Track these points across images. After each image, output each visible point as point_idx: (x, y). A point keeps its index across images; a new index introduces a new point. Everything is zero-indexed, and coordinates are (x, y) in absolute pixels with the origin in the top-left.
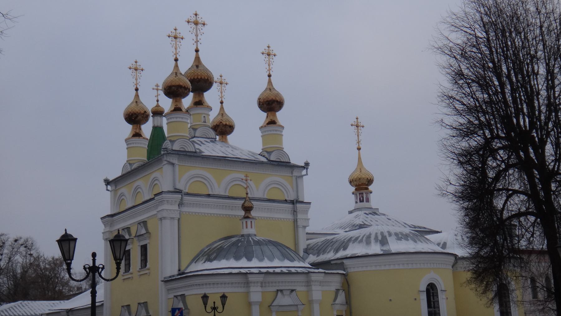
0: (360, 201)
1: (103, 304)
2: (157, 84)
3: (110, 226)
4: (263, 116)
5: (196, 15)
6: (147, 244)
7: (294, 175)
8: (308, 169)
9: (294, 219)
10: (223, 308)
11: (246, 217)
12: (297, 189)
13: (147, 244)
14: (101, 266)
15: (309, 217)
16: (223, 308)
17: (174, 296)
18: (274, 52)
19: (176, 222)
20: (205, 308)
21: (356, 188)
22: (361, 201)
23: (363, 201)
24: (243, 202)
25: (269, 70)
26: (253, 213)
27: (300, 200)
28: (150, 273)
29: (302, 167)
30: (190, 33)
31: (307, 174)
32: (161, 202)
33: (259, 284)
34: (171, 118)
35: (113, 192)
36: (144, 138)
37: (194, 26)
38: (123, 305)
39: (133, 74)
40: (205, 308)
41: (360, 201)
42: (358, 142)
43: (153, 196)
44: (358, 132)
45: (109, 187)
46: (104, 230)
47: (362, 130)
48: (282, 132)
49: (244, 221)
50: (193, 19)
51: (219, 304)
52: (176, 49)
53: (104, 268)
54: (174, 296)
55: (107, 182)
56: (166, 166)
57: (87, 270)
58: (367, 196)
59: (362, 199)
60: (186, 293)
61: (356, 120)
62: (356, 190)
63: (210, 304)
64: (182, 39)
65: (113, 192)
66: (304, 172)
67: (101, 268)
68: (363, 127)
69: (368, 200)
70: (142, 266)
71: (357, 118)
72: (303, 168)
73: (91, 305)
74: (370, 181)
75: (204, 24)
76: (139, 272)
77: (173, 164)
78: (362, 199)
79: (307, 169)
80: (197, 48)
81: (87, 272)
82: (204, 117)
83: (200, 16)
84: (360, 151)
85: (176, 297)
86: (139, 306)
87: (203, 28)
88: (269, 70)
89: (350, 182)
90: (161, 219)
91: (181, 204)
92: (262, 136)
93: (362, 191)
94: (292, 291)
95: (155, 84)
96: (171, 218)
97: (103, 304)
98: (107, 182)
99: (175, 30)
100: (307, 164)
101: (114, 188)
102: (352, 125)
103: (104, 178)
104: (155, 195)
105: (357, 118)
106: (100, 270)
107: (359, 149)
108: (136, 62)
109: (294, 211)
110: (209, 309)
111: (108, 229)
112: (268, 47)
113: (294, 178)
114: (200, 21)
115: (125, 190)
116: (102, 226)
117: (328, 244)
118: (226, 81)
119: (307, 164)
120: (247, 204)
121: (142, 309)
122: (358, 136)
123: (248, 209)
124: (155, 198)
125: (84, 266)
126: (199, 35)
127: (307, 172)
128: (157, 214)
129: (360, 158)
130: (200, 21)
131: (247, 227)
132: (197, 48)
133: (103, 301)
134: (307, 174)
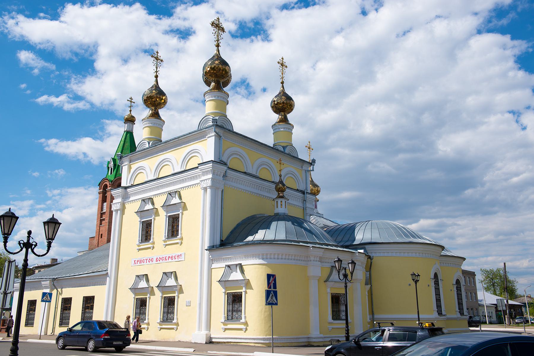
2: (131, 98)
4: (275, 117)
7: (303, 169)
9: (304, 208)
14: (34, 243)
17: (226, 266)
18: (286, 64)
31: (313, 170)
39: (154, 62)
49: (279, 200)
52: (157, 68)
53: (37, 246)
54: (226, 266)
57: (22, 245)
58: (315, 203)
60: (243, 263)
67: (34, 245)
73: (26, 278)
81: (21, 246)
85: (229, 266)
86: (165, 276)
95: (130, 97)
100: (314, 161)
106: (33, 246)
113: (304, 172)
119: (314, 161)
124: (199, 168)
125: (19, 242)
127: (313, 168)
128: (200, 183)
134: (313, 170)
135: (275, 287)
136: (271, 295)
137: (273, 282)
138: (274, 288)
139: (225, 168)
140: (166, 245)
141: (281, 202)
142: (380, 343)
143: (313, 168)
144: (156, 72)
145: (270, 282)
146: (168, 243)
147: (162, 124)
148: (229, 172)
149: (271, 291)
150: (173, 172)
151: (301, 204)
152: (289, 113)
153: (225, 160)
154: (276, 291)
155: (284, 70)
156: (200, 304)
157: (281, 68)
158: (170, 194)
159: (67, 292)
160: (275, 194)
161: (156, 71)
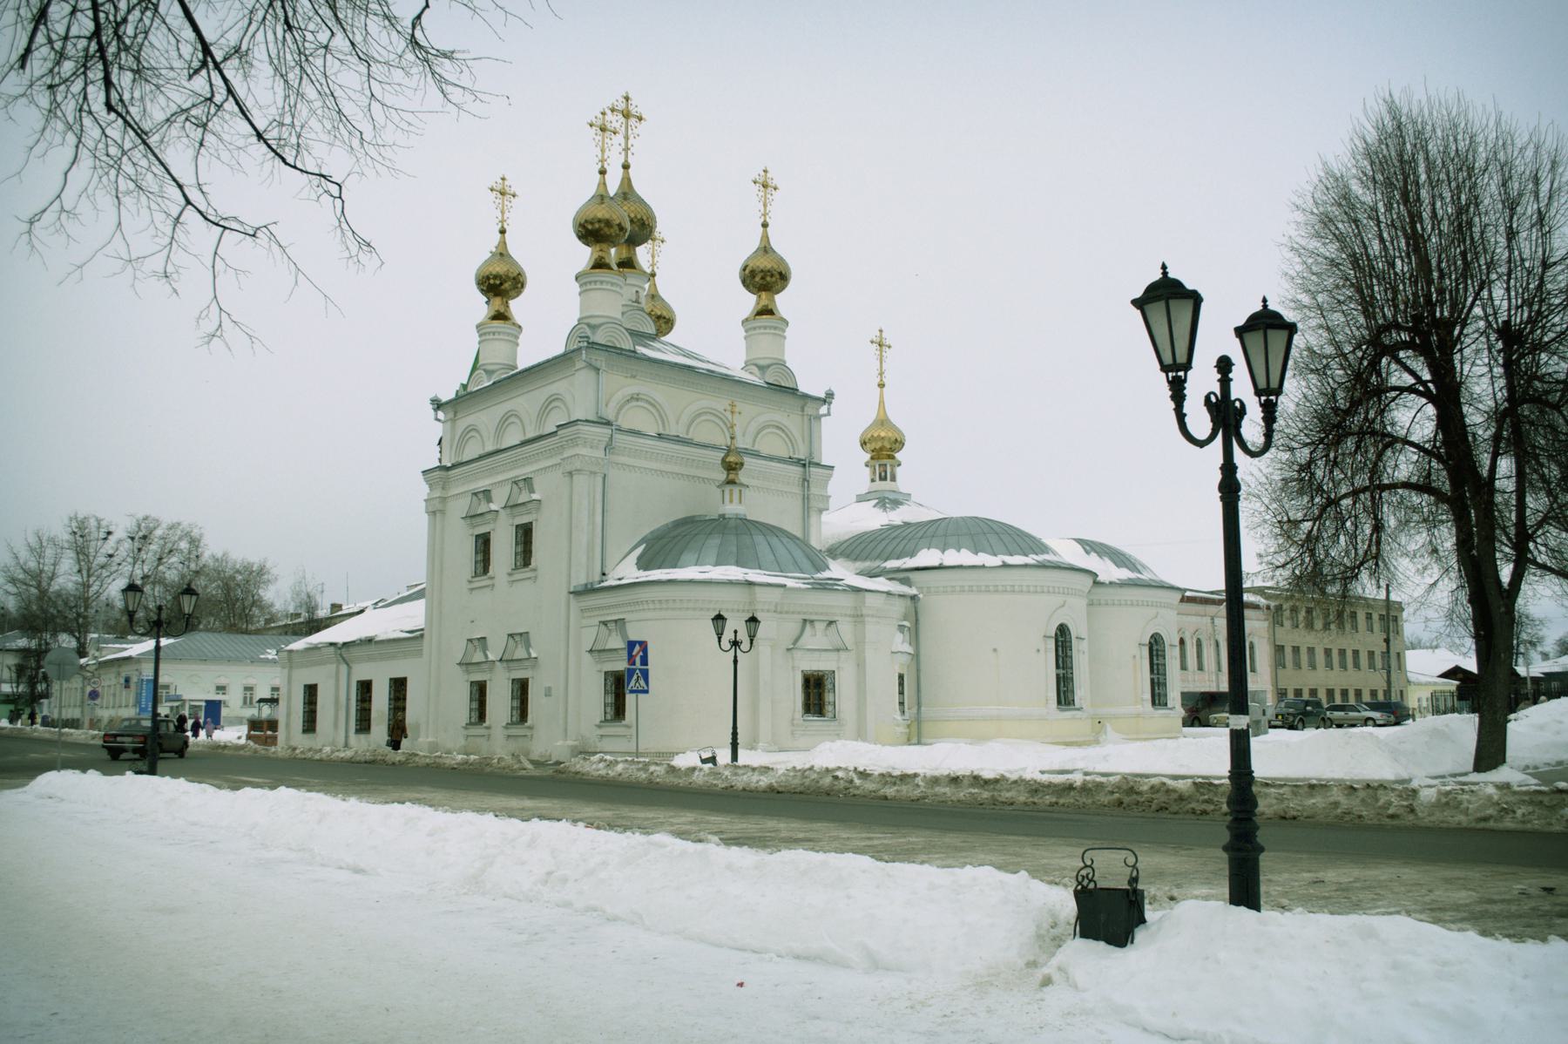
0: (881, 479)
1: (422, 636)
3: (443, 488)
5: (627, 99)
6: (531, 523)
8: (832, 406)
10: (751, 643)
11: (731, 482)
12: (811, 437)
13: (531, 523)
15: (829, 494)
16: (751, 643)
18: (775, 182)
19: (599, 480)
20: (720, 641)
21: (21, 662)
22: (883, 478)
23: (885, 479)
24: (723, 455)
25: (765, 215)
26: (742, 477)
27: (815, 460)
28: (493, 585)
29: (818, 399)
30: (594, 144)
32: (574, 441)
33: (932, 590)
34: (590, 283)
35: (449, 423)
36: (514, 324)
37: (623, 120)
38: (510, 632)
39: (497, 201)
40: (720, 641)
41: (881, 479)
42: (881, 374)
43: (555, 429)
44: (881, 356)
45: (441, 415)
46: (428, 494)
47: (888, 353)
48: (784, 331)
49: (727, 489)
50: (621, 106)
51: (743, 636)
52: (503, 213)
55: (438, 405)
56: (583, 372)
59: (883, 474)
60: (627, 617)
61: (878, 334)
62: (872, 458)
63: (728, 635)
64: (514, 196)
65: (449, 423)
66: (823, 410)
68: (889, 347)
69: (893, 479)
70: (518, 564)
71: (881, 331)
72: (825, 401)
74: (899, 443)
75: (640, 119)
76: (470, 582)
77: (597, 370)
78: (883, 474)
79: (830, 403)
80: (626, 161)
82: (637, 292)
83: (634, 102)
84: (884, 389)
85: (605, 623)
87: (638, 124)
88: (765, 215)
89: (864, 444)
90: (571, 474)
91: (609, 447)
92: (746, 338)
93: (885, 461)
94: (831, 623)
96: (591, 472)
97: (422, 636)
98: (438, 405)
99: (503, 179)
100: (830, 395)
101: (451, 415)
102: (872, 342)
103: (432, 396)
104: (558, 426)
105: (881, 331)
107: (881, 386)
108: (503, 179)
109: (804, 480)
110: (726, 644)
111: (437, 494)
112: (765, 171)
113: (806, 418)
114: (633, 110)
115: (485, 418)
116: (425, 488)
117: (863, 546)
118: (662, 235)
119: (830, 395)
120: (731, 459)
121: (475, 651)
122: (881, 363)
123: (731, 467)
124: (559, 433)
126: (631, 137)
127: (829, 409)
129: (882, 403)
130: (633, 112)
131: (731, 501)
132: (626, 161)
133: (422, 630)
135: (644, 661)
136: (635, 677)
137: (641, 654)
138: (642, 665)
139: (607, 431)
140: (472, 589)
141: (731, 490)
142: (133, 743)
143: (829, 409)
144: (602, 161)
145: (634, 653)
146: (517, 576)
147: (515, 333)
148: (617, 436)
149: (635, 670)
150: (482, 452)
151: (797, 490)
152: (778, 292)
153: (611, 417)
154: (647, 670)
155: (769, 196)
156: (348, 699)
157: (761, 194)
158: (516, 482)
159: (362, 672)
160: (722, 476)
161: (623, 146)
